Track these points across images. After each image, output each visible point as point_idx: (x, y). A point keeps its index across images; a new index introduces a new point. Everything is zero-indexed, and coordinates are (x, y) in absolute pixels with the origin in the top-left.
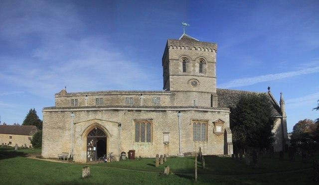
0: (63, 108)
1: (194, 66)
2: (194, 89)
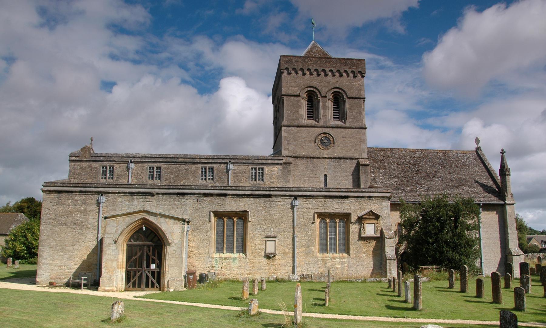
0: (85, 185)
1: (325, 108)
2: (325, 154)
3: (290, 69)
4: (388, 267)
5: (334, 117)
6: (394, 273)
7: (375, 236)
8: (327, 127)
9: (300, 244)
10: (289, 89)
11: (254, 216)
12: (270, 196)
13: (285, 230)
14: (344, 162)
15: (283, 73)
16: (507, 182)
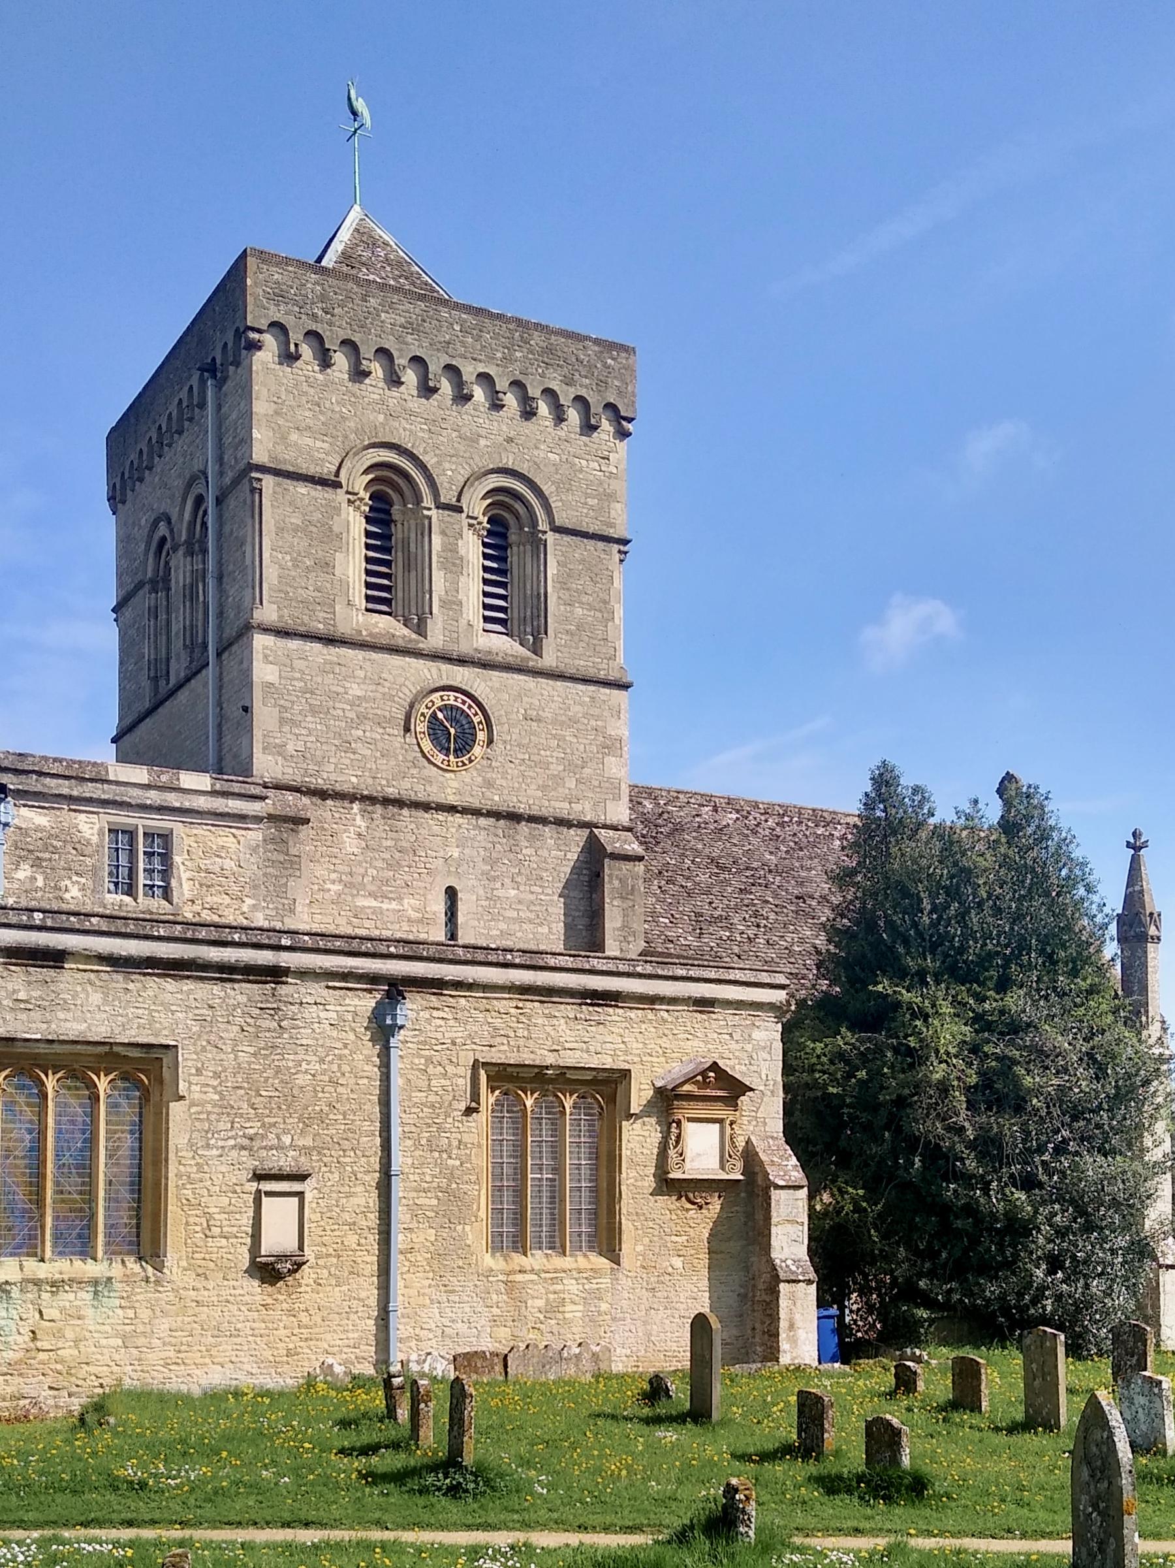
1: (455, 565)
3: (295, 336)
4: (783, 1314)
5: (488, 613)
6: (807, 1338)
7: (724, 1176)
8: (462, 661)
9: (415, 1211)
10: (284, 438)
11: (199, 1072)
12: (276, 974)
13: (346, 1145)
14: (532, 838)
15: (256, 346)
16: (1150, 969)
